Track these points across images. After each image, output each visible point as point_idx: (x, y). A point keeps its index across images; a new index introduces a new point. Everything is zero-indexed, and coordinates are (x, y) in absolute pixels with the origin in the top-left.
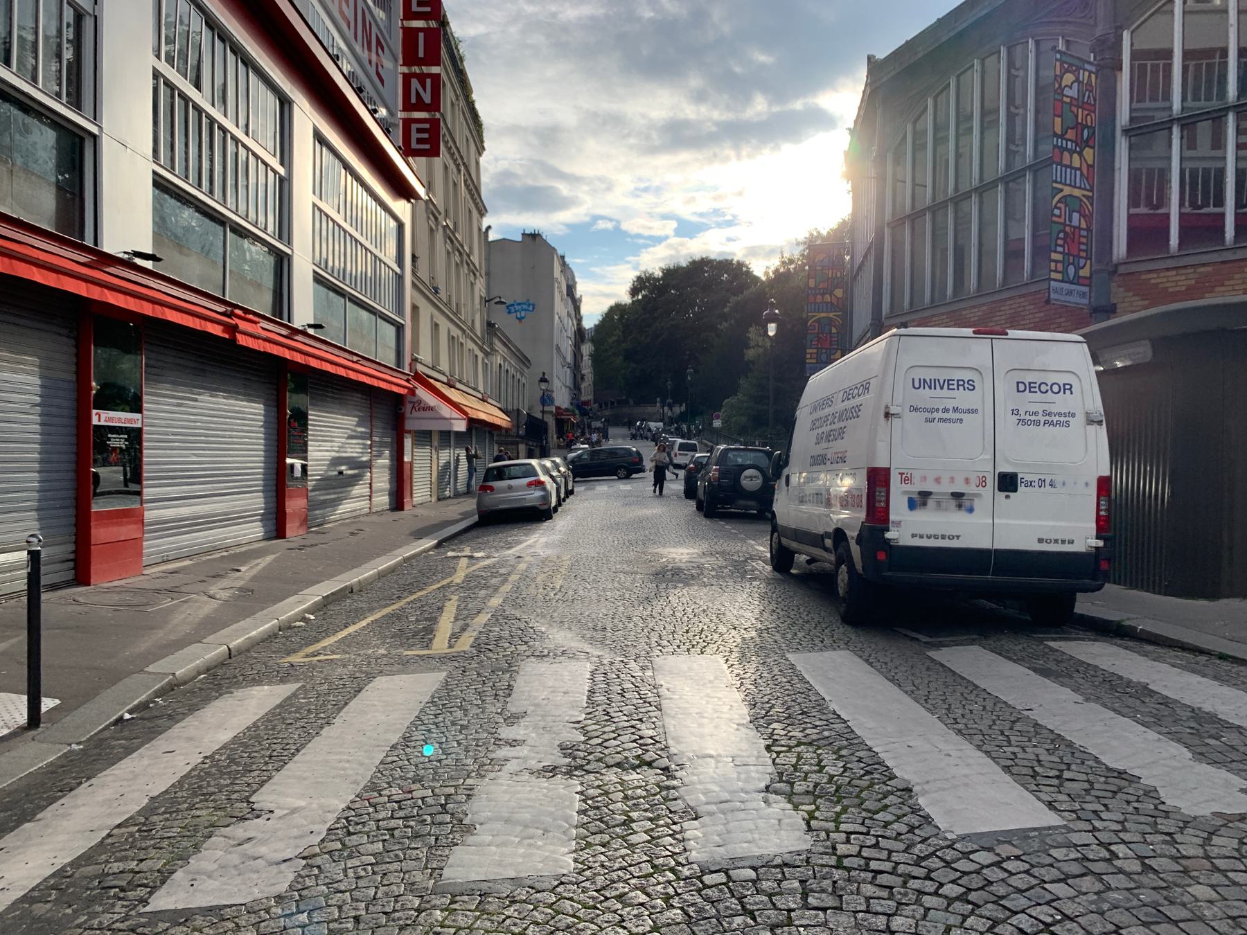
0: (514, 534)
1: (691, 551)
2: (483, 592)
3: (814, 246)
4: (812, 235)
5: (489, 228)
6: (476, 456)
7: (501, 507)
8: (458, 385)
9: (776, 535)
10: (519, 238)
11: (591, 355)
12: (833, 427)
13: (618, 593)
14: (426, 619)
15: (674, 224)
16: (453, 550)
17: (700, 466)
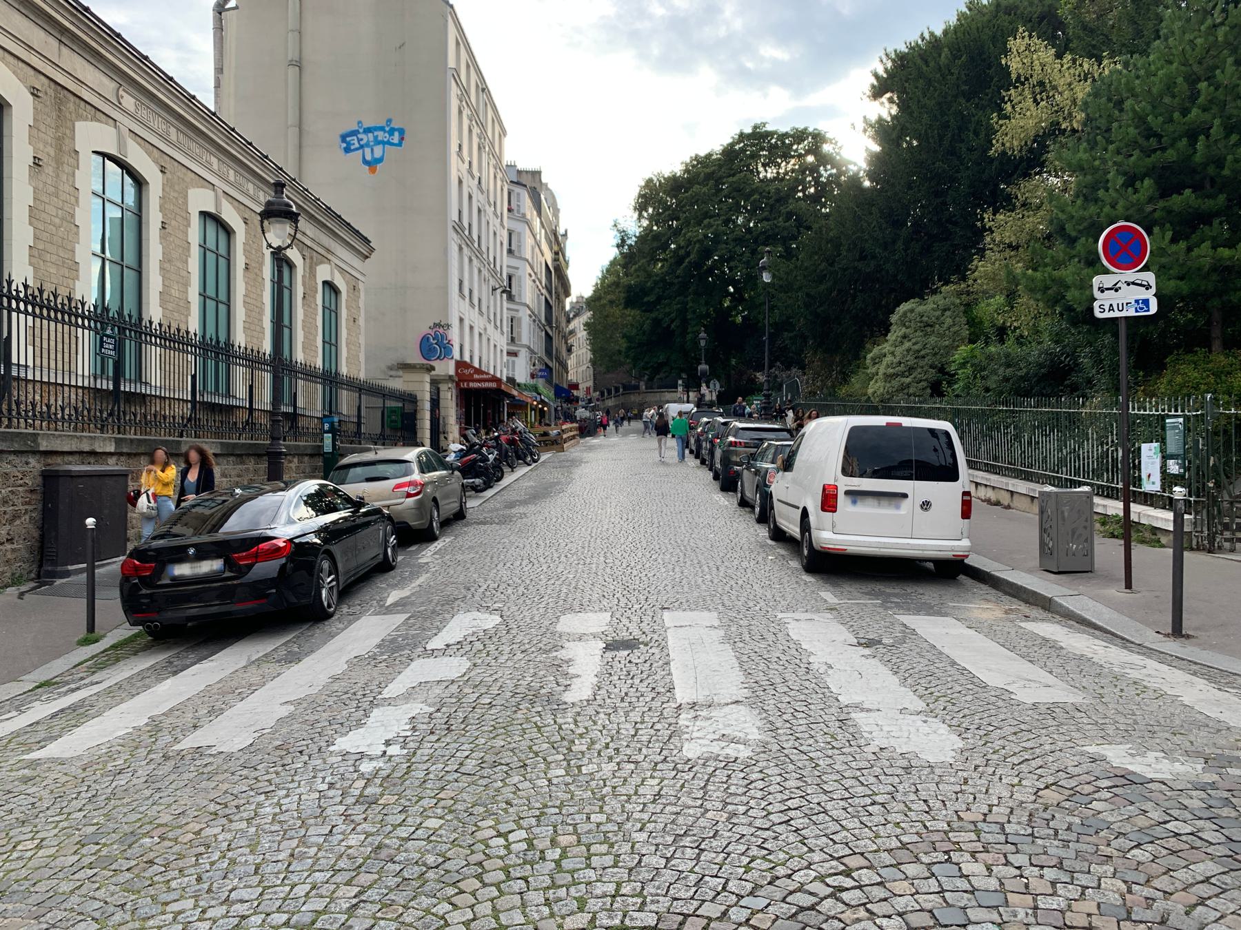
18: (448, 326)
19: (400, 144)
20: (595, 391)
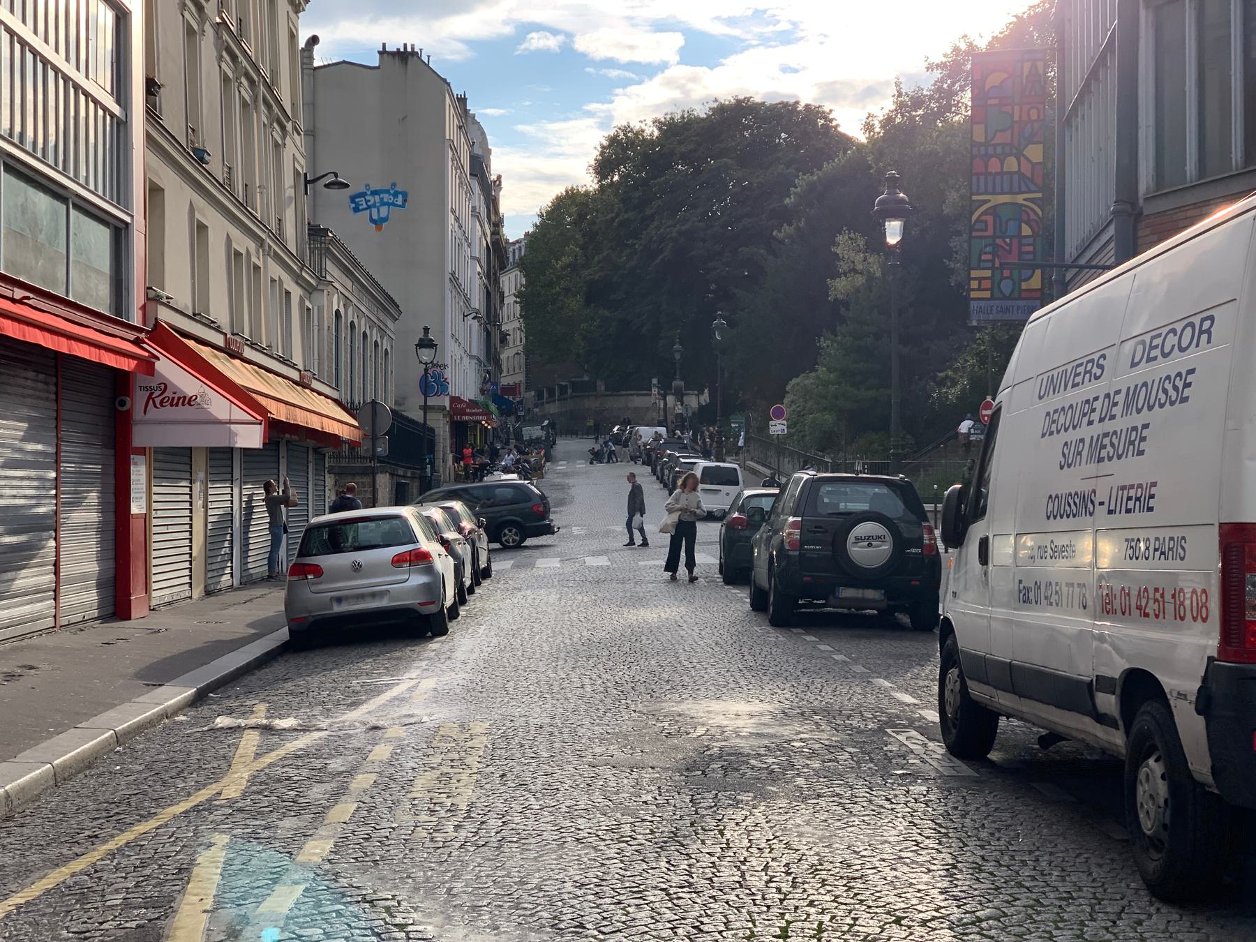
0: (363, 669)
1: (756, 707)
2: (287, 823)
3: (962, 66)
4: (956, 50)
5: (314, 40)
6: (285, 500)
7: (337, 609)
8: (248, 353)
9: (953, 673)
10: (375, 61)
11: (519, 295)
12: (1109, 426)
13: (605, 822)
14: (149, 903)
15: (678, 40)
16: (230, 712)
17: (756, 517)
18: (445, 366)
19: (403, 206)
20: (528, 389)
